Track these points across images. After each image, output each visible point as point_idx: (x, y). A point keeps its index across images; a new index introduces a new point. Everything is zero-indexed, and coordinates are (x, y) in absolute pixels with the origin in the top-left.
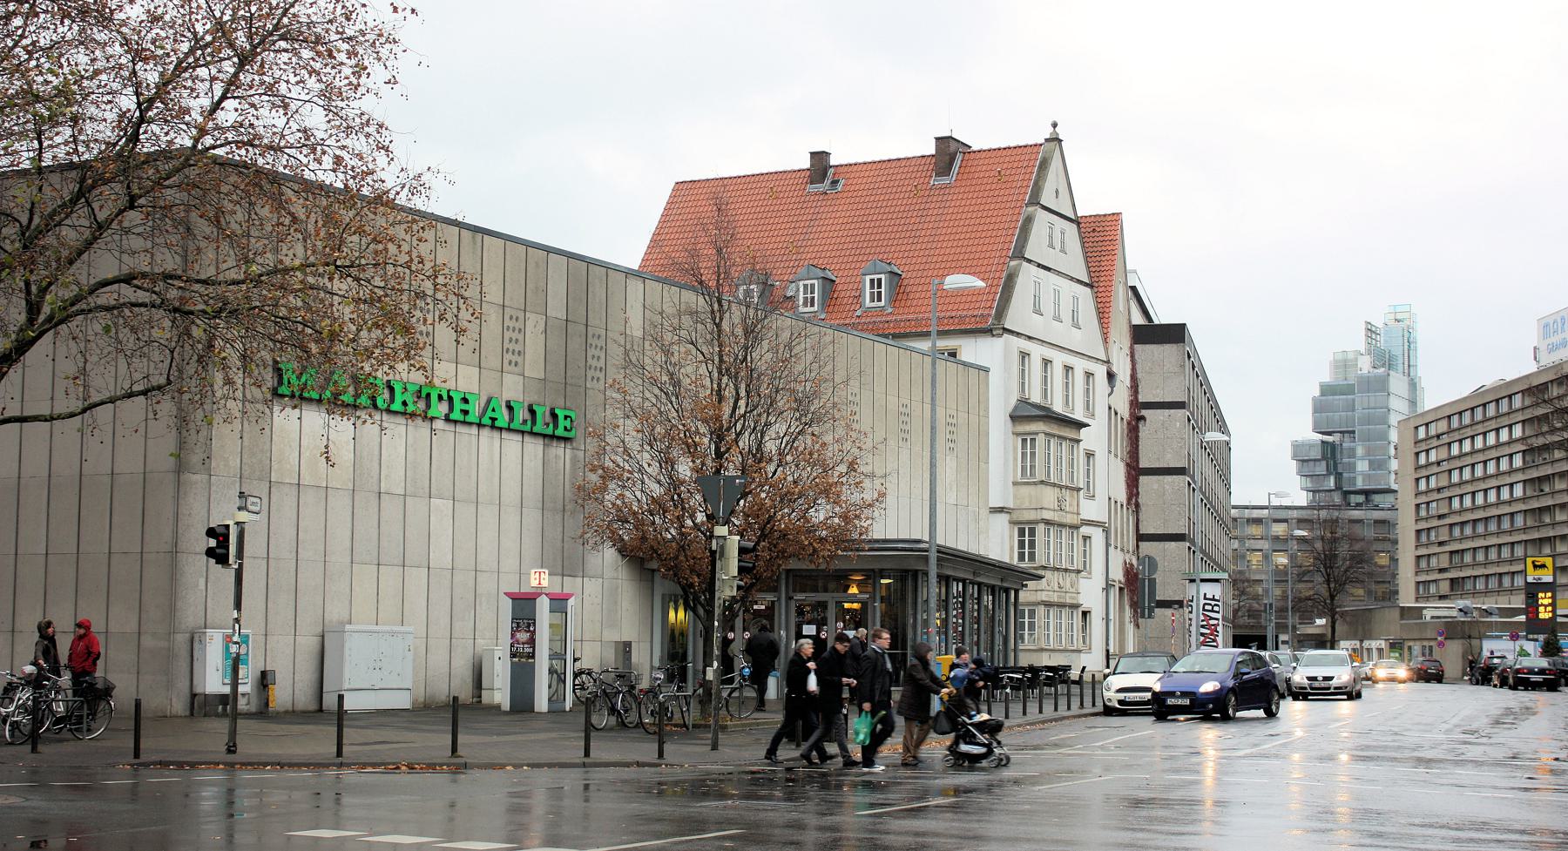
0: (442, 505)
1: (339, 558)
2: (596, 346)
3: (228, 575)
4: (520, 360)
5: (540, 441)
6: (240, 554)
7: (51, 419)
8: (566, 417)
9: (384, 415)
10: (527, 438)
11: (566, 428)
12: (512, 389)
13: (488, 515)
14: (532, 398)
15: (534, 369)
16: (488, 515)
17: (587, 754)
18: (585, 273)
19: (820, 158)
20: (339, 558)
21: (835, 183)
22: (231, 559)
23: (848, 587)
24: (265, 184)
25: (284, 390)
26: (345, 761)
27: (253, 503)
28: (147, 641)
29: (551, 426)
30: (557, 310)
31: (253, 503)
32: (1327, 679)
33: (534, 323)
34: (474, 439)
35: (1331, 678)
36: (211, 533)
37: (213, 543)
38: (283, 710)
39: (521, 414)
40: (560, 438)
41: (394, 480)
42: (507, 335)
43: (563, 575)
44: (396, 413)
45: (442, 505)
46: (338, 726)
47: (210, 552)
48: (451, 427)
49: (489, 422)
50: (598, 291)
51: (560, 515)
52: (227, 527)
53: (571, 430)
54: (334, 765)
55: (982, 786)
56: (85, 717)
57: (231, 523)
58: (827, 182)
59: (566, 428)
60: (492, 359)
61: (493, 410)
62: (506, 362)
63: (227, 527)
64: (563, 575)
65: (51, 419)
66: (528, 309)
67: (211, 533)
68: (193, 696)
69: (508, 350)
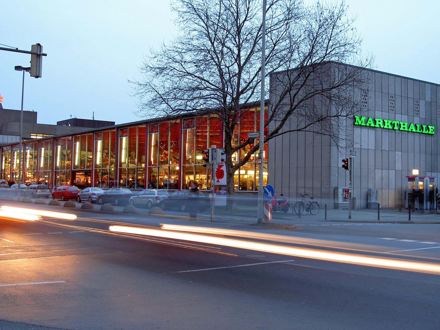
0: (399, 153)
2: (392, 100)
3: (348, 172)
4: (418, 113)
5: (425, 135)
6: (351, 167)
7: (290, 131)
8: (432, 128)
9: (383, 129)
10: (421, 135)
11: (432, 132)
13: (411, 155)
16: (411, 155)
17: (410, 219)
18: (435, 88)
22: (349, 168)
26: (380, 221)
27: (354, 153)
28: (323, 190)
29: (422, 130)
30: (428, 99)
31: (354, 153)
33: (422, 103)
34: (407, 135)
36: (343, 161)
37: (344, 164)
38: (125, 194)
40: (430, 134)
42: (415, 106)
43: (432, 172)
44: (386, 129)
46: (325, 210)
47: (343, 166)
49: (369, 125)
51: (431, 155)
52: (347, 159)
53: (433, 132)
54: (377, 222)
55: (377, 223)
57: (348, 158)
59: (432, 132)
60: (411, 113)
61: (412, 127)
62: (390, 110)
63: (347, 159)
64: (432, 172)
65: (290, 131)
66: (420, 99)
67: (343, 161)
68: (335, 204)
69: (390, 106)
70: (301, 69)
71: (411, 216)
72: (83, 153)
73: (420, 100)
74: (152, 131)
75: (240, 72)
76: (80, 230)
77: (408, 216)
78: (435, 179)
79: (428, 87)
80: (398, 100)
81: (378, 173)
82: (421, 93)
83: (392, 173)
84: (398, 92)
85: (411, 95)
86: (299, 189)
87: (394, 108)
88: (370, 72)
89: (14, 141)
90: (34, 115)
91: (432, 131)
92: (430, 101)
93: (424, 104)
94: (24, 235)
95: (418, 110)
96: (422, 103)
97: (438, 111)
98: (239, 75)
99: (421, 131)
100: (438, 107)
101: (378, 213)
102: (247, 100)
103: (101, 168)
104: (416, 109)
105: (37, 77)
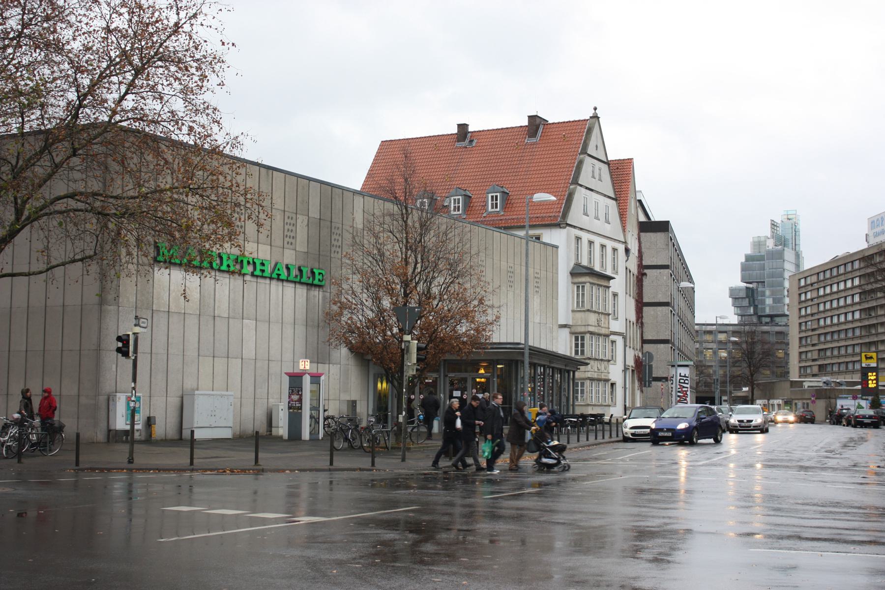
0: (249, 323)
1: (191, 352)
2: (337, 234)
3: (129, 363)
10: (298, 286)
12: (289, 257)
13: (275, 329)
15: (301, 247)
16: (275, 329)
17: (331, 464)
19: (463, 127)
20: (191, 352)
21: (471, 141)
25: (160, 258)
28: (83, 400)
29: (311, 279)
30: (314, 213)
31: (143, 322)
33: (302, 221)
34: (268, 286)
36: (119, 339)
37: (120, 345)
39: (294, 272)
41: (222, 309)
42: (286, 227)
45: (249, 323)
47: (119, 350)
51: (316, 329)
54: (189, 470)
57: (130, 333)
58: (467, 141)
59: (319, 280)
60: (278, 242)
67: (119, 339)
71: (260, 455)
73: (298, 216)
77: (253, 455)
78: (322, 378)
79: (315, 188)
82: (299, 199)
86: (601, 428)
87: (269, 237)
88: (263, 170)
91: (321, 279)
92: (319, 218)
93: (306, 222)
95: (292, 234)
97: (333, 238)
99: (310, 281)
100: (333, 230)
101: (254, 454)
104: (289, 234)
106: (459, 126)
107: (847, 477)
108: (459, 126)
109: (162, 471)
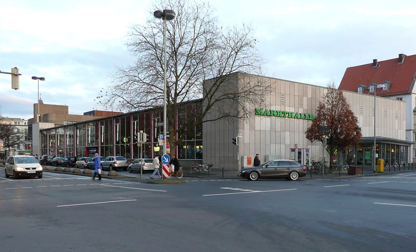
1: (268, 143)
12: (301, 111)
13: (297, 135)
14: (305, 113)
15: (305, 107)
16: (297, 135)
19: (375, 61)
20: (268, 143)
21: (378, 66)
23: (198, 145)
24: (237, 80)
25: (257, 114)
30: (310, 96)
32: (33, 169)
33: (305, 99)
35: (35, 168)
39: (303, 116)
41: (278, 128)
45: (287, 133)
47: (233, 143)
48: (289, 119)
50: (318, 91)
56: (63, 159)
58: (376, 66)
60: (297, 106)
70: (216, 79)
72: (160, 124)
74: (116, 123)
75: (177, 81)
76: (129, 183)
80: (287, 97)
81: (273, 146)
83: (283, 146)
84: (287, 92)
85: (297, 94)
89: (50, 127)
90: (66, 108)
94: (284, 172)
96: (305, 99)
98: (176, 83)
102: (183, 100)
103: (120, 145)
105: (16, 89)
106: (399, 55)
107: (143, 182)
108: (399, 55)
109: (307, 176)
